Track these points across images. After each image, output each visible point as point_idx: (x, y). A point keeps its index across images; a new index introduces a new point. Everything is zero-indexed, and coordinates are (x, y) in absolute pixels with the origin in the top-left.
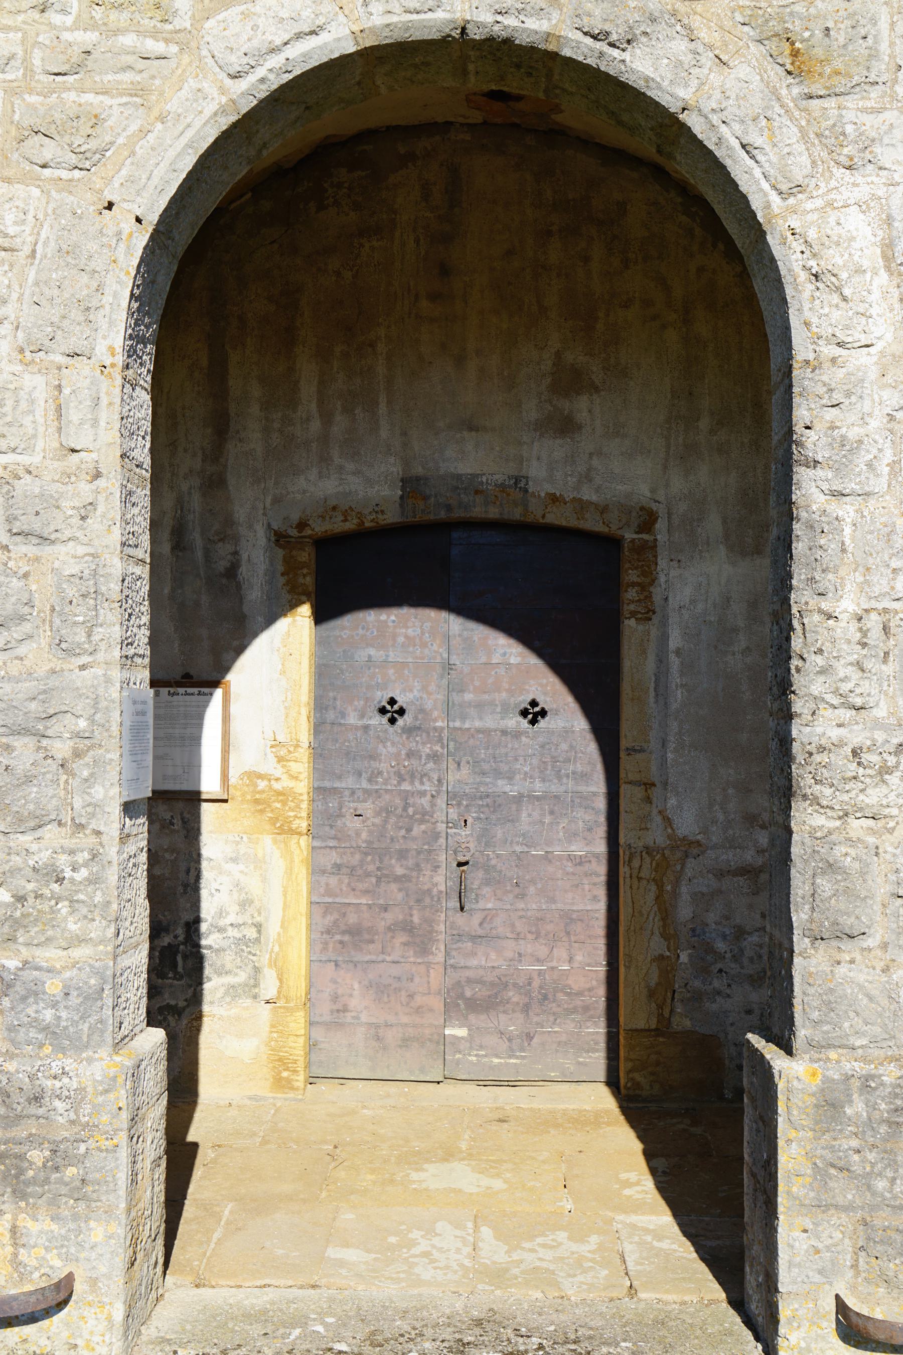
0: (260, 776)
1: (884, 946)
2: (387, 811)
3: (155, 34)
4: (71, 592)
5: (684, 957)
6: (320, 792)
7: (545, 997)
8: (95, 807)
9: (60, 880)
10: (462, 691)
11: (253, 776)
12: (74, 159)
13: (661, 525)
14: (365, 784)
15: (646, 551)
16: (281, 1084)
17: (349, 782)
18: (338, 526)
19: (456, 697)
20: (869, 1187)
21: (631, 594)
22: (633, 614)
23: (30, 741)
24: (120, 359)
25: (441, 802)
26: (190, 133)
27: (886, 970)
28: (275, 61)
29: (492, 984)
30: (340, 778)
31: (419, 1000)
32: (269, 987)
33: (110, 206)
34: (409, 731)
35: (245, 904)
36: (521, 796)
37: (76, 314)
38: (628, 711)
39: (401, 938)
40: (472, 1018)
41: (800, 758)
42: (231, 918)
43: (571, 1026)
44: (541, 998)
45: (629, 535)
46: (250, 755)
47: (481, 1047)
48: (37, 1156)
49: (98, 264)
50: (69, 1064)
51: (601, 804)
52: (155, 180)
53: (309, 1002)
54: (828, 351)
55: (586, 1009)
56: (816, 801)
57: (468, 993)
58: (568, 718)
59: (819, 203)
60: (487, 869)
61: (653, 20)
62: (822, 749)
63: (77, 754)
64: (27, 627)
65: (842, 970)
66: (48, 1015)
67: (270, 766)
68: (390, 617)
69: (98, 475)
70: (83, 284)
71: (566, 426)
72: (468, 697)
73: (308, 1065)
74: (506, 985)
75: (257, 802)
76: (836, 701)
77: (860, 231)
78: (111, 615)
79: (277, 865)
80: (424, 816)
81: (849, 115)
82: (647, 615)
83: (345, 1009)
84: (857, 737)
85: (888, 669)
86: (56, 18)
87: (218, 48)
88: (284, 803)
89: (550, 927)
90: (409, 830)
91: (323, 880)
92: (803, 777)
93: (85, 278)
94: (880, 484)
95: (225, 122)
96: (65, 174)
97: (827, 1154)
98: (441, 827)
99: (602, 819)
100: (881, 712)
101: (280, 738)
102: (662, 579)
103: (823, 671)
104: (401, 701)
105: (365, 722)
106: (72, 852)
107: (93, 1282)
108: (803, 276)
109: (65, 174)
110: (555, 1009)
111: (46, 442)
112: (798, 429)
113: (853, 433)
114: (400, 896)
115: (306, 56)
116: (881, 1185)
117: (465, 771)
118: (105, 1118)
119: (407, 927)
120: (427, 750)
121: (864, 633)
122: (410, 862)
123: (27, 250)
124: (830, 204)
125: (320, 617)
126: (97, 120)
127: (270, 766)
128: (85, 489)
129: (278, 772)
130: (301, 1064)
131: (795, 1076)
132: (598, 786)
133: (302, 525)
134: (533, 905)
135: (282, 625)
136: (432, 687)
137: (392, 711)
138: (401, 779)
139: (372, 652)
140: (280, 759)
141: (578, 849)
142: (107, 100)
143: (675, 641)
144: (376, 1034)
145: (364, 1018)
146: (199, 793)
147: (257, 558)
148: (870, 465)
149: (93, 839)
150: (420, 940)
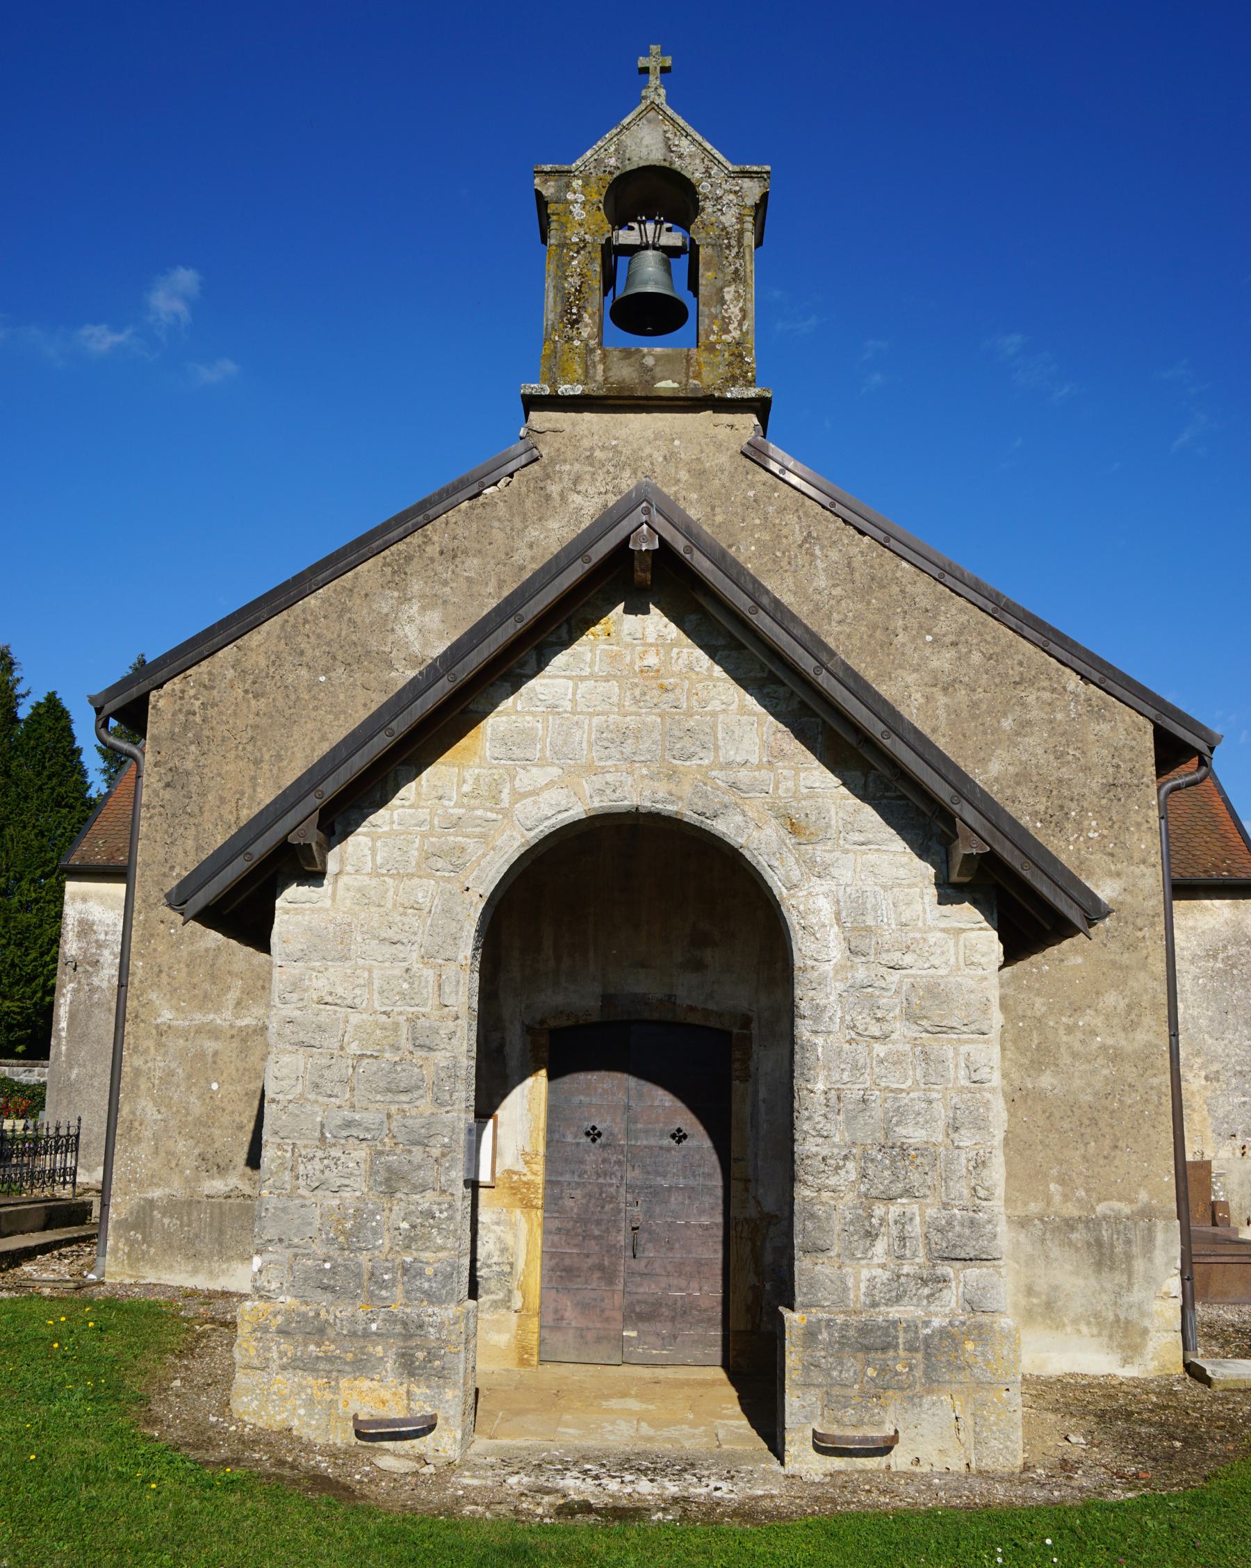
0: (515, 1173)
1: (839, 1256)
2: (589, 1196)
3: (492, 810)
4: (443, 1075)
5: (768, 1286)
6: (549, 1183)
7: (685, 1312)
8: (452, 1182)
9: (433, 1218)
10: (636, 1122)
11: (510, 1172)
12: (451, 868)
13: (754, 1025)
14: (576, 1179)
15: (746, 1040)
16: (523, 1362)
17: (567, 1177)
18: (564, 1022)
19: (632, 1126)
20: (829, 1375)
21: (736, 1065)
22: (738, 1078)
23: (420, 1148)
24: (469, 962)
25: (623, 1190)
26: (507, 856)
27: (840, 1267)
28: (547, 823)
29: (653, 1304)
30: (561, 1174)
31: (607, 1313)
32: (517, 1302)
33: (468, 889)
34: (603, 1146)
35: (504, 1250)
36: (671, 1187)
37: (449, 941)
38: (735, 1135)
39: (597, 1274)
40: (640, 1325)
41: (798, 1162)
42: (495, 1259)
43: (700, 1331)
44: (683, 1312)
45: (735, 1031)
46: (509, 1160)
47: (645, 1343)
48: (420, 1355)
49: (460, 917)
50: (436, 1310)
51: (719, 1192)
52: (489, 878)
53: (541, 1314)
54: (810, 963)
55: (710, 1320)
56: (805, 1183)
57: (638, 1310)
58: (700, 1140)
59: (805, 893)
60: (650, 1232)
61: (726, 807)
62: (808, 1157)
63: (443, 1155)
64: (421, 1092)
65: (818, 1268)
66: (426, 1285)
67: (520, 1167)
68: (593, 1077)
69: (457, 1018)
71: (698, 966)
72: (640, 1126)
73: (539, 1353)
74: (661, 1305)
75: (512, 1188)
76: (814, 1133)
77: (825, 907)
78: (461, 1086)
79: (523, 1226)
80: (612, 1199)
81: (818, 853)
82: (746, 1078)
83: (562, 1319)
84: (825, 1151)
85: (841, 1118)
86: (446, 803)
87: (521, 817)
88: (528, 1189)
89: (688, 1269)
90: (603, 1207)
91: (550, 1237)
92: (800, 1171)
93: (454, 923)
94: (835, 1027)
95: (523, 850)
96: (447, 874)
97: (810, 1359)
98: (622, 1205)
99: (720, 1201)
100: (837, 1139)
101: (527, 1149)
102: (755, 1056)
103: (809, 1119)
104: (599, 1128)
105: (577, 1140)
106: (439, 1204)
107: (447, 1419)
108: (797, 927)
109: (447, 874)
110: (691, 1320)
111: (433, 1001)
112: (797, 1000)
113: (823, 1002)
114: (597, 1248)
115: (562, 820)
116: (835, 1373)
117: (637, 1171)
118: (454, 1337)
119: (600, 1267)
120: (614, 1158)
121: (828, 1100)
122: (604, 1227)
123: (427, 909)
124: (810, 893)
125: (551, 1077)
126: (463, 849)
127: (520, 1167)
128: (451, 1024)
129: (525, 1170)
130: (535, 1351)
131: (794, 1319)
132: (718, 1181)
133: (542, 1022)
134: (678, 1255)
135: (529, 1081)
136: (618, 1120)
137: (593, 1134)
138: (599, 1176)
139: (582, 1098)
140: (526, 1163)
141: (705, 1221)
142: (468, 840)
143: (763, 1094)
144: (581, 1333)
145: (574, 1324)
146: (478, 1182)
148: (830, 1018)
149: (450, 1198)
150: (609, 1276)
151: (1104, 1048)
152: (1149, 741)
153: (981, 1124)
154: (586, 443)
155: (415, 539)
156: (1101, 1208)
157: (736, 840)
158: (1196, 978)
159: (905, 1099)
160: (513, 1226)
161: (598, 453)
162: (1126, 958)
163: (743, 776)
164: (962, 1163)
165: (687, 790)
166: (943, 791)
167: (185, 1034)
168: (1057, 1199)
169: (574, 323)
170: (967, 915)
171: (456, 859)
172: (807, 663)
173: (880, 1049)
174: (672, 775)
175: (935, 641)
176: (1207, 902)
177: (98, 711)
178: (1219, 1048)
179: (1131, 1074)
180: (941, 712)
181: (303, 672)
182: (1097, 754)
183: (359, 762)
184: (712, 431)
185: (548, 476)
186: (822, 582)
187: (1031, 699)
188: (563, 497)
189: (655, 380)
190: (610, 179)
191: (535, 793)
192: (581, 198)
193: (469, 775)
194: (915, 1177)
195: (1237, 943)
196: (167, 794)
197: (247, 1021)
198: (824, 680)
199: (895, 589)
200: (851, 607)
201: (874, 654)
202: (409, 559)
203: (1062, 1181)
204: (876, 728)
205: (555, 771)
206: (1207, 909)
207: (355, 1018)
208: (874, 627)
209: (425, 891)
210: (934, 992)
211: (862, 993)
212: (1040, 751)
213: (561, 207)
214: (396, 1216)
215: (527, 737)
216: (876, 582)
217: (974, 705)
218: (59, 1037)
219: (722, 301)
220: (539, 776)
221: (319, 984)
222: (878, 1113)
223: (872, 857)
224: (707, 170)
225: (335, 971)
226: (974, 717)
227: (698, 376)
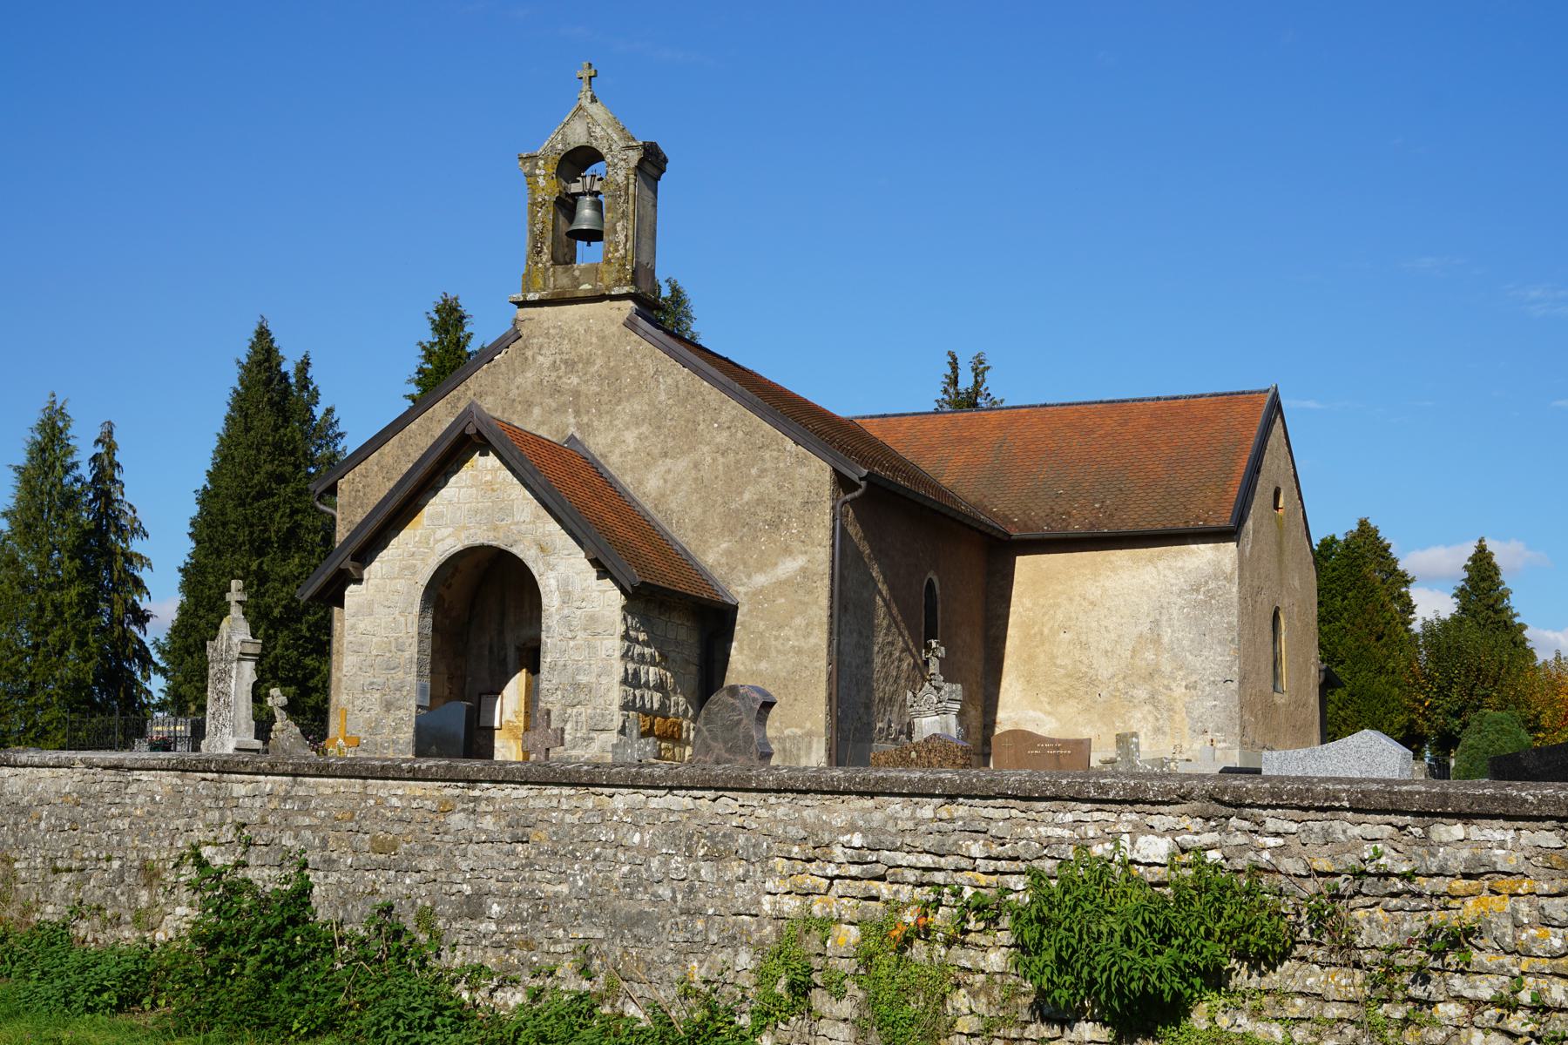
77: (553, 582)
79: (515, 748)
147: (512, 654)
151: (793, 647)
156: (787, 732)
160: (510, 749)
161: (552, 331)
162: (806, 599)
163: (523, 527)
171: (413, 570)
173: (572, 643)
174: (495, 529)
176: (1194, 547)
178: (1197, 663)
179: (806, 660)
182: (800, 485)
186: (663, 397)
195: (1216, 578)
205: (450, 530)
206: (1193, 552)
208: (688, 421)
209: (400, 584)
210: (592, 619)
214: (390, 721)
215: (442, 515)
219: (615, 232)
220: (446, 532)
221: (361, 626)
225: (368, 620)
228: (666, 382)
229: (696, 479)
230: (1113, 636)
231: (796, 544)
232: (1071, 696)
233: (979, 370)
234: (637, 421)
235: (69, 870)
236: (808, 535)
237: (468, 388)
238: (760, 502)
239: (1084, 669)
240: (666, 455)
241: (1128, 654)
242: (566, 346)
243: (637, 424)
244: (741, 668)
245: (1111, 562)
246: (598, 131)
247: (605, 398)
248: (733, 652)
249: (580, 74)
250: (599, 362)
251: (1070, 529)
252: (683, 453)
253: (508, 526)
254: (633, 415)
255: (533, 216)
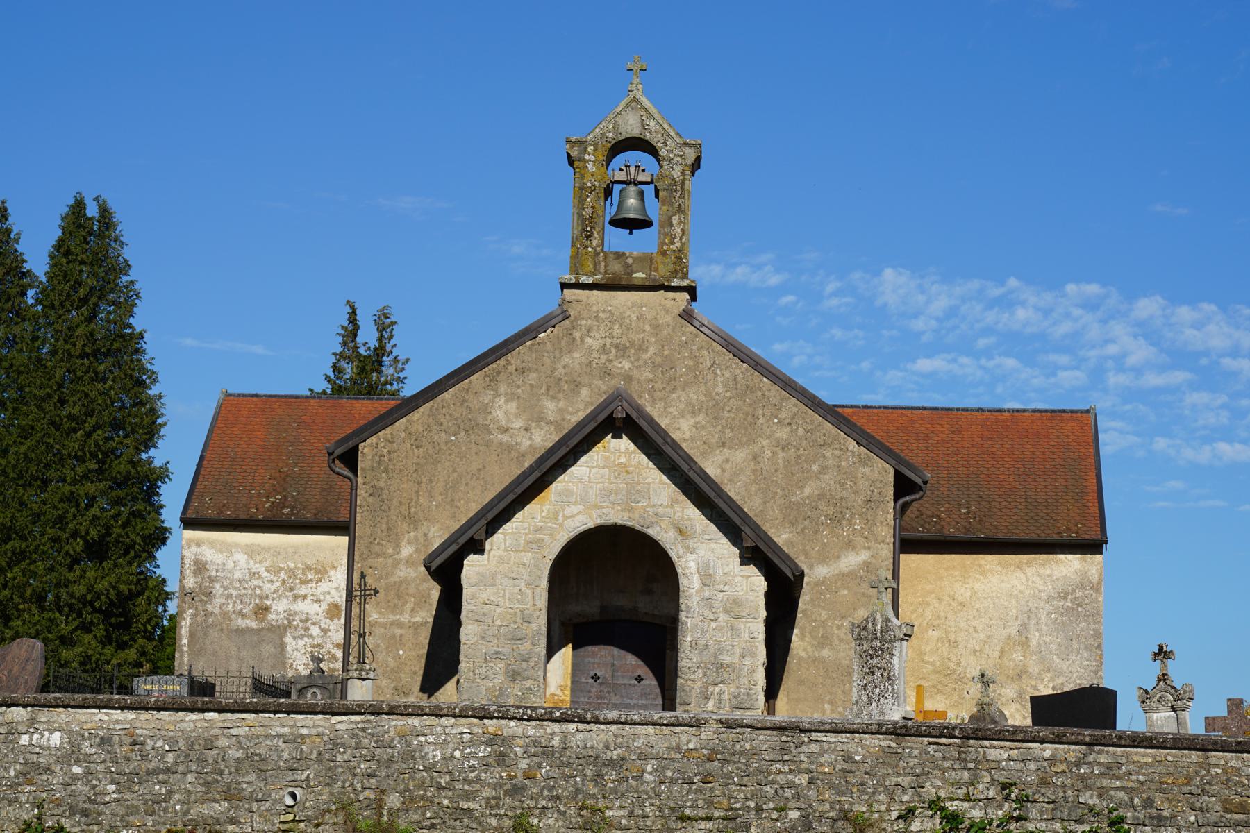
11: (553, 695)
34: (601, 684)
58: (651, 682)
67: (559, 692)
68: (595, 648)
70: (539, 573)
71: (649, 592)
77: (693, 566)
92: (679, 673)
111: (531, 603)
125: (574, 649)
127: (559, 692)
135: (563, 650)
137: (596, 678)
152: (891, 478)
153: (753, 655)
154: (595, 308)
155: (502, 362)
157: (657, 538)
158: (1050, 613)
159: (723, 644)
161: (601, 315)
163: (660, 509)
164: (746, 671)
165: (637, 516)
166: (738, 521)
167: (384, 626)
168: (828, 712)
169: (588, 237)
170: (752, 570)
171: (539, 543)
172: (685, 467)
173: (713, 625)
174: (630, 510)
175: (779, 422)
176: (1062, 556)
177: (330, 454)
178: (1064, 666)
180: (780, 461)
181: (443, 435)
182: (863, 484)
183: (502, 506)
184: (664, 302)
185: (574, 327)
186: (720, 389)
187: (829, 454)
188: (582, 340)
189: (633, 272)
190: (609, 145)
191: (573, 517)
192: (593, 158)
193: (546, 508)
194: (726, 676)
195: (1084, 588)
196: (371, 500)
197: (417, 619)
198: (691, 474)
199: (759, 393)
200: (734, 403)
201: (746, 429)
202: (499, 373)
203: (831, 703)
204: (712, 495)
205: (581, 507)
207: (498, 610)
208: (747, 414)
209: (527, 557)
210: (736, 602)
211: (707, 602)
212: (832, 482)
213: (581, 164)
215: (569, 493)
216: (749, 389)
217: (799, 457)
218: (182, 651)
219: (671, 225)
220: (574, 509)
221: (483, 596)
222: (712, 650)
223: (713, 545)
224: (665, 142)
225: (490, 590)
226: (798, 464)
227: (656, 270)
228: (723, 375)
229: (754, 471)
230: (982, 636)
231: (859, 540)
232: (939, 692)
233: (384, 325)
234: (692, 409)
235: (709, 818)
236: (871, 532)
237: (509, 363)
238: (821, 497)
239: (952, 666)
240: (724, 445)
241: (997, 654)
242: (616, 330)
243: (693, 414)
244: (803, 654)
245: (980, 566)
246: (652, 125)
247: (659, 385)
248: (794, 638)
249: (630, 66)
250: (652, 350)
251: (946, 533)
252: (742, 444)
253: (644, 508)
254: (689, 404)
255: (582, 201)
